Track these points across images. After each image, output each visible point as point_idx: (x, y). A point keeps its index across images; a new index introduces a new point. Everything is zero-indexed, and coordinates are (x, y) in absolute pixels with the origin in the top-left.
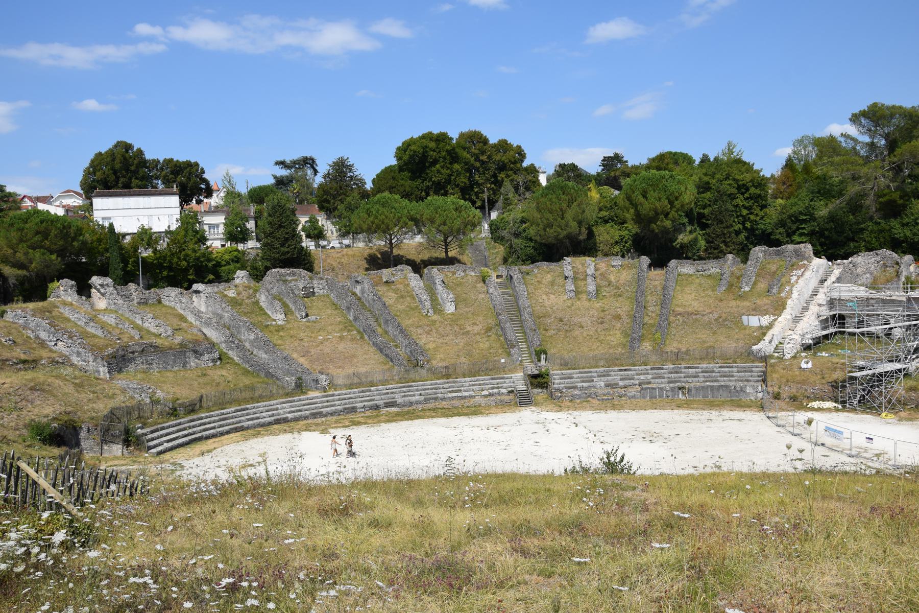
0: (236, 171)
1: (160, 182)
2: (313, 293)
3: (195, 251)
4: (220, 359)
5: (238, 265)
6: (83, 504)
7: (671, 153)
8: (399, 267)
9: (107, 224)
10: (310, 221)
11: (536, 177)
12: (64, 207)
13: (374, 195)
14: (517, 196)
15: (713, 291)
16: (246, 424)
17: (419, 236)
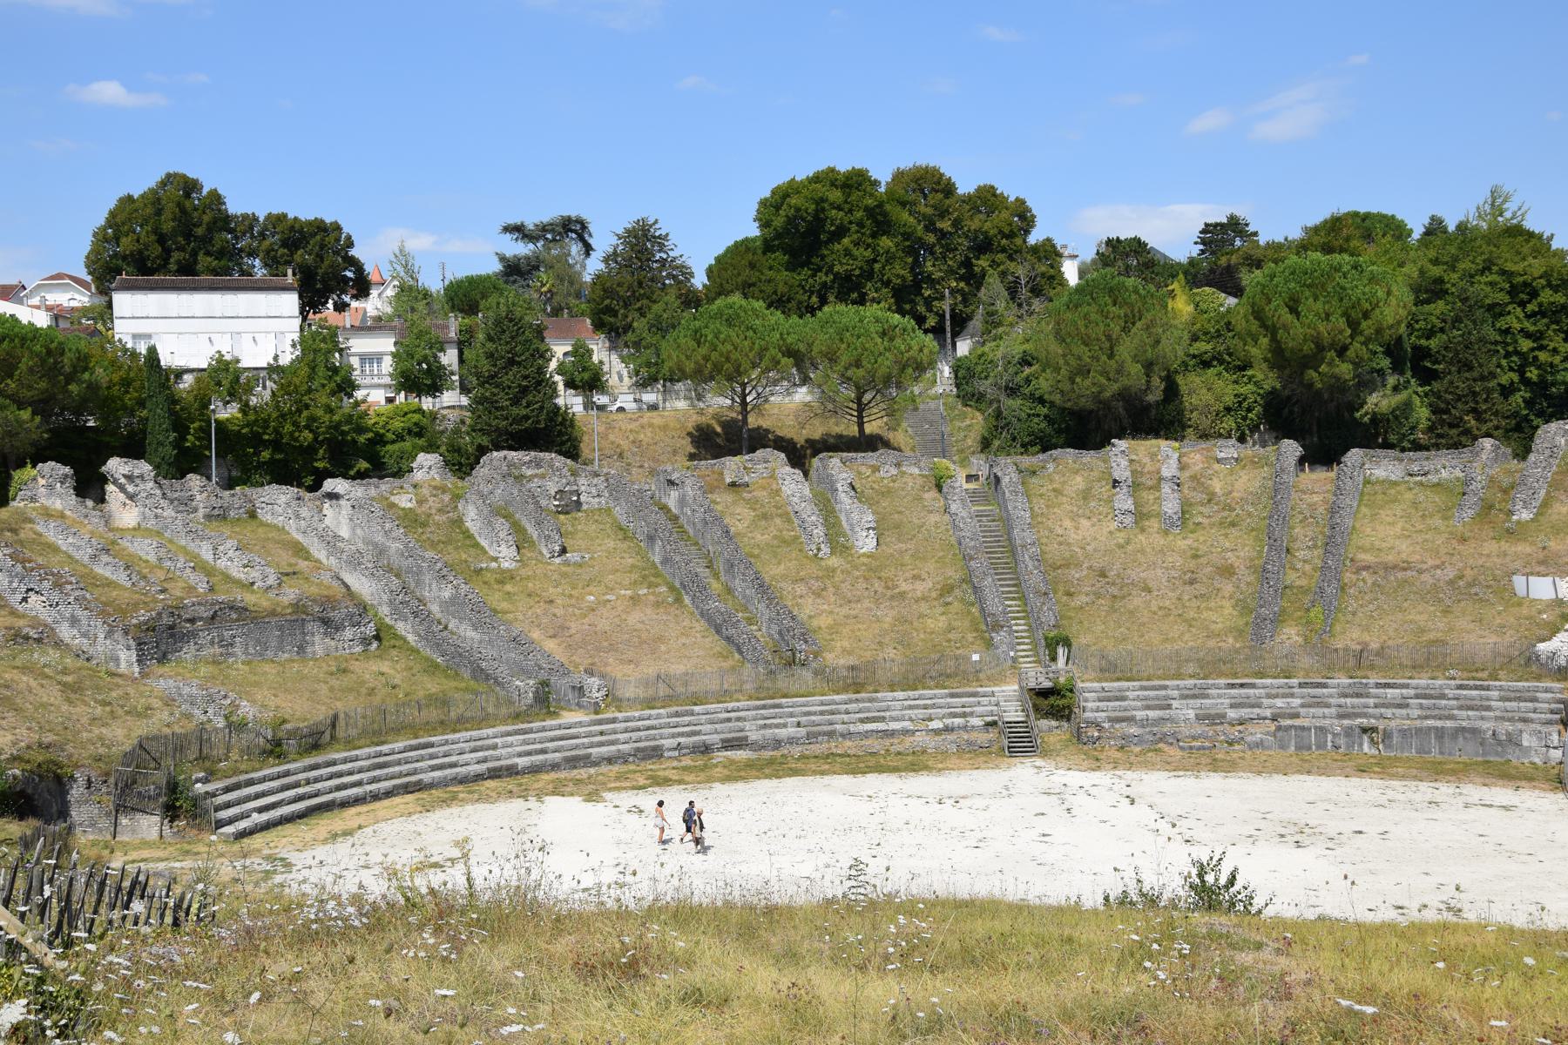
0: (419, 244)
1: (257, 262)
2: (579, 503)
3: (330, 410)
4: (377, 637)
5: (422, 442)
6: (68, 944)
7: (1356, 214)
8: (760, 453)
9: (142, 349)
10: (574, 353)
11: (1056, 267)
12: (49, 309)
13: (711, 300)
14: (1014, 306)
15: (1445, 518)
16: (427, 777)
17: (804, 389)
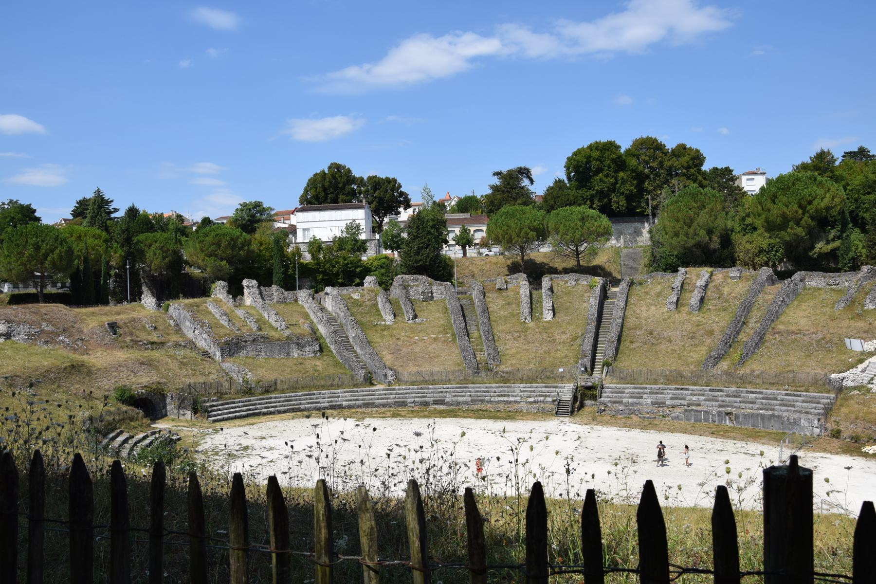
2: (432, 297)
16: (302, 407)
